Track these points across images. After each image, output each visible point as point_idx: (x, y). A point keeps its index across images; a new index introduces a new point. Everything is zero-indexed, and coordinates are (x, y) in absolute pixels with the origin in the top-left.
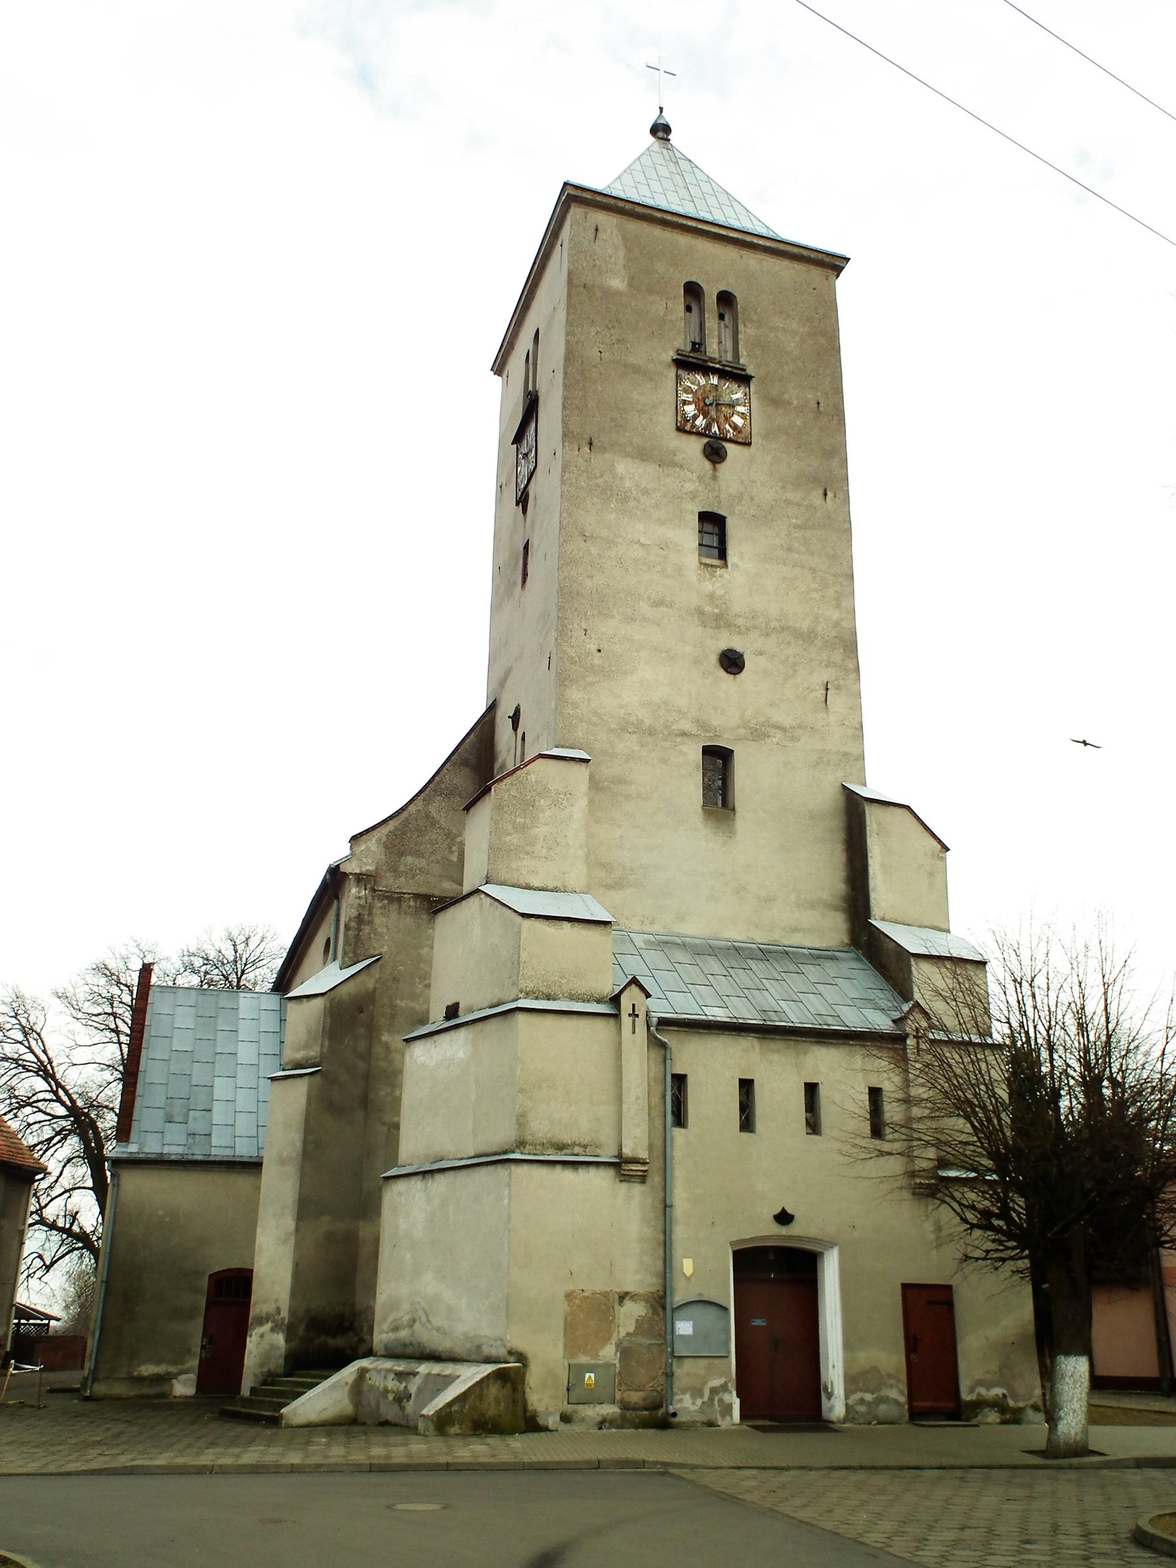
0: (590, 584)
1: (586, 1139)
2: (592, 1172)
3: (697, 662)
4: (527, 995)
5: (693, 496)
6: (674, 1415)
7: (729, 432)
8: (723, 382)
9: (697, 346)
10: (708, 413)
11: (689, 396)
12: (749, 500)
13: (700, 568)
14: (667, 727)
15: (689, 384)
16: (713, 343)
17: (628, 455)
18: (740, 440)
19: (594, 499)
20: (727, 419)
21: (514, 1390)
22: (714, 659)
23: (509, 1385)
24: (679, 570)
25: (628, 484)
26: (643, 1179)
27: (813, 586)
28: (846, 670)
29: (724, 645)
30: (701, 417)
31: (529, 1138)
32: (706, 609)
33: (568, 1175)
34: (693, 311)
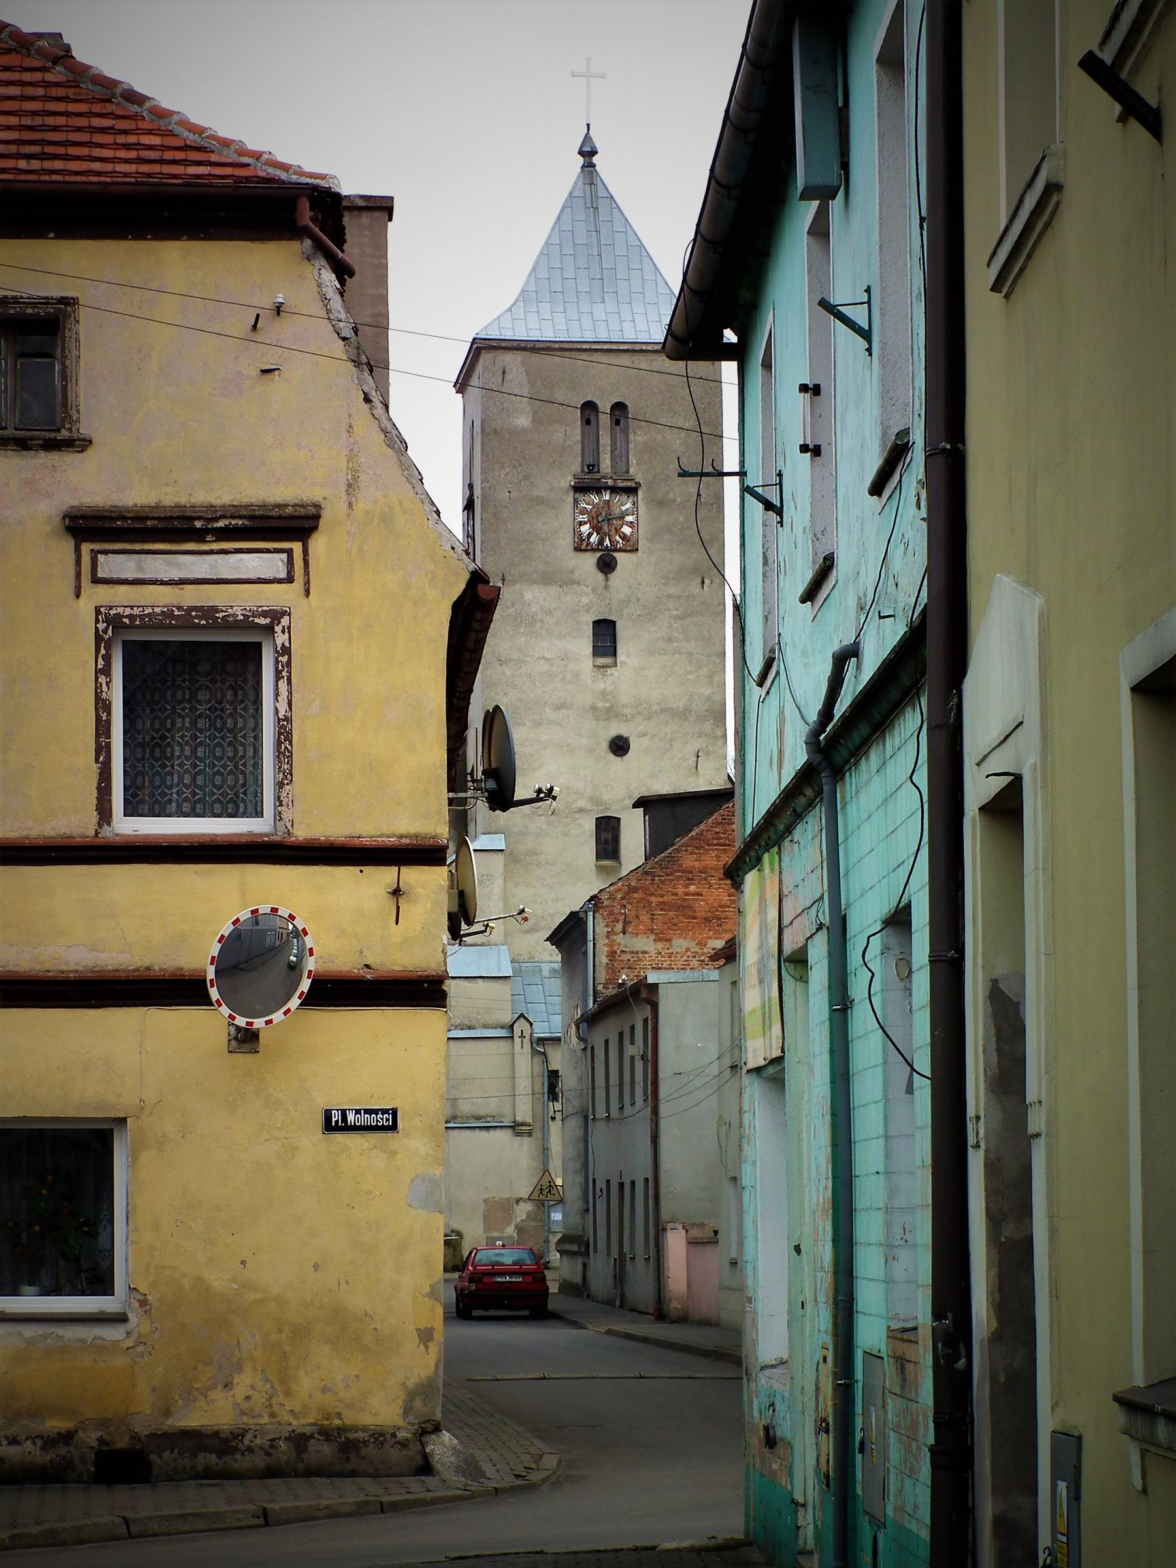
0: (506, 700)
1: (493, 1113)
2: (498, 1131)
3: (591, 751)
4: (456, 1027)
5: (588, 608)
6: (548, 1262)
7: (619, 542)
8: (614, 495)
9: (592, 468)
10: (601, 528)
11: (584, 516)
12: (636, 601)
13: (593, 671)
14: (567, 807)
15: (585, 505)
16: (606, 458)
17: (533, 582)
18: (628, 548)
19: (508, 627)
20: (617, 531)
21: (454, 1250)
22: (605, 746)
23: (452, 1248)
24: (577, 675)
25: (534, 609)
26: (530, 1134)
27: (689, 669)
28: (715, 738)
29: (613, 733)
30: (595, 534)
31: (459, 1114)
32: (599, 705)
33: (484, 1134)
34: (592, 424)
